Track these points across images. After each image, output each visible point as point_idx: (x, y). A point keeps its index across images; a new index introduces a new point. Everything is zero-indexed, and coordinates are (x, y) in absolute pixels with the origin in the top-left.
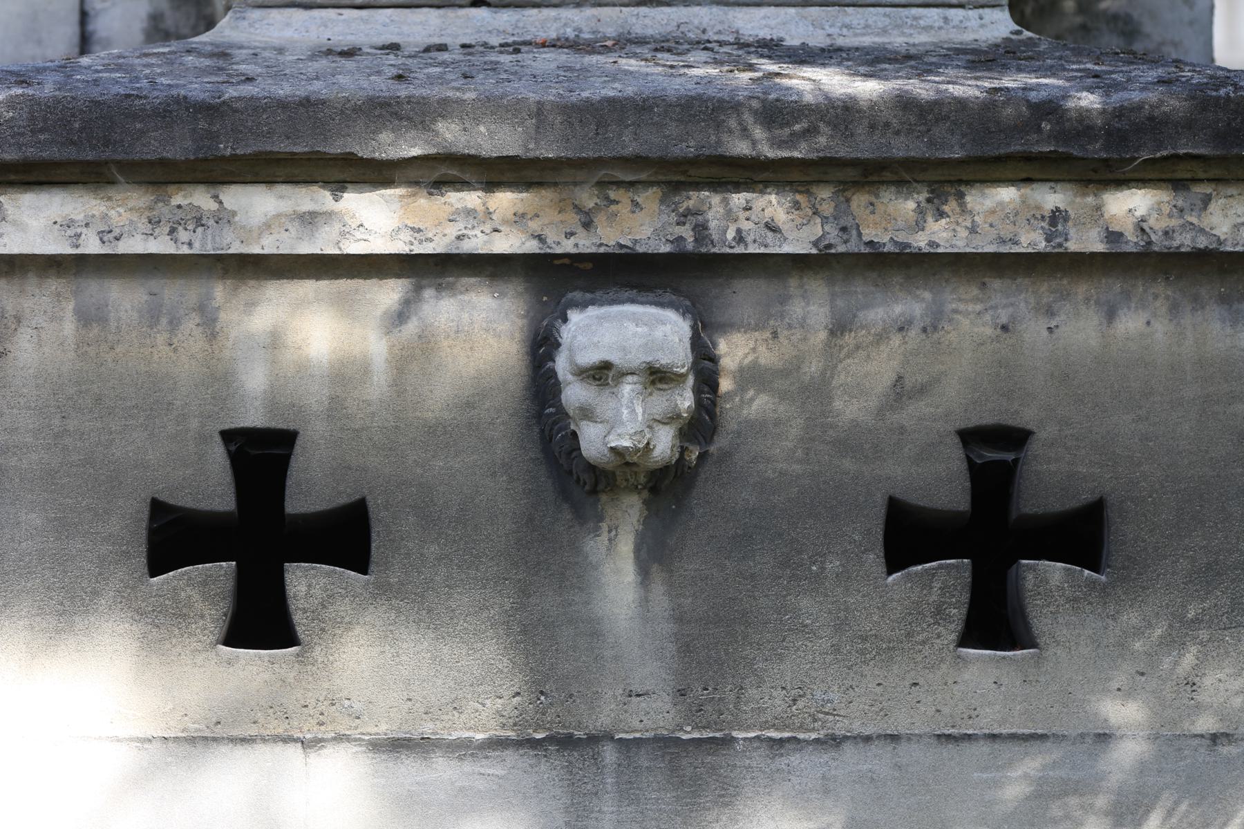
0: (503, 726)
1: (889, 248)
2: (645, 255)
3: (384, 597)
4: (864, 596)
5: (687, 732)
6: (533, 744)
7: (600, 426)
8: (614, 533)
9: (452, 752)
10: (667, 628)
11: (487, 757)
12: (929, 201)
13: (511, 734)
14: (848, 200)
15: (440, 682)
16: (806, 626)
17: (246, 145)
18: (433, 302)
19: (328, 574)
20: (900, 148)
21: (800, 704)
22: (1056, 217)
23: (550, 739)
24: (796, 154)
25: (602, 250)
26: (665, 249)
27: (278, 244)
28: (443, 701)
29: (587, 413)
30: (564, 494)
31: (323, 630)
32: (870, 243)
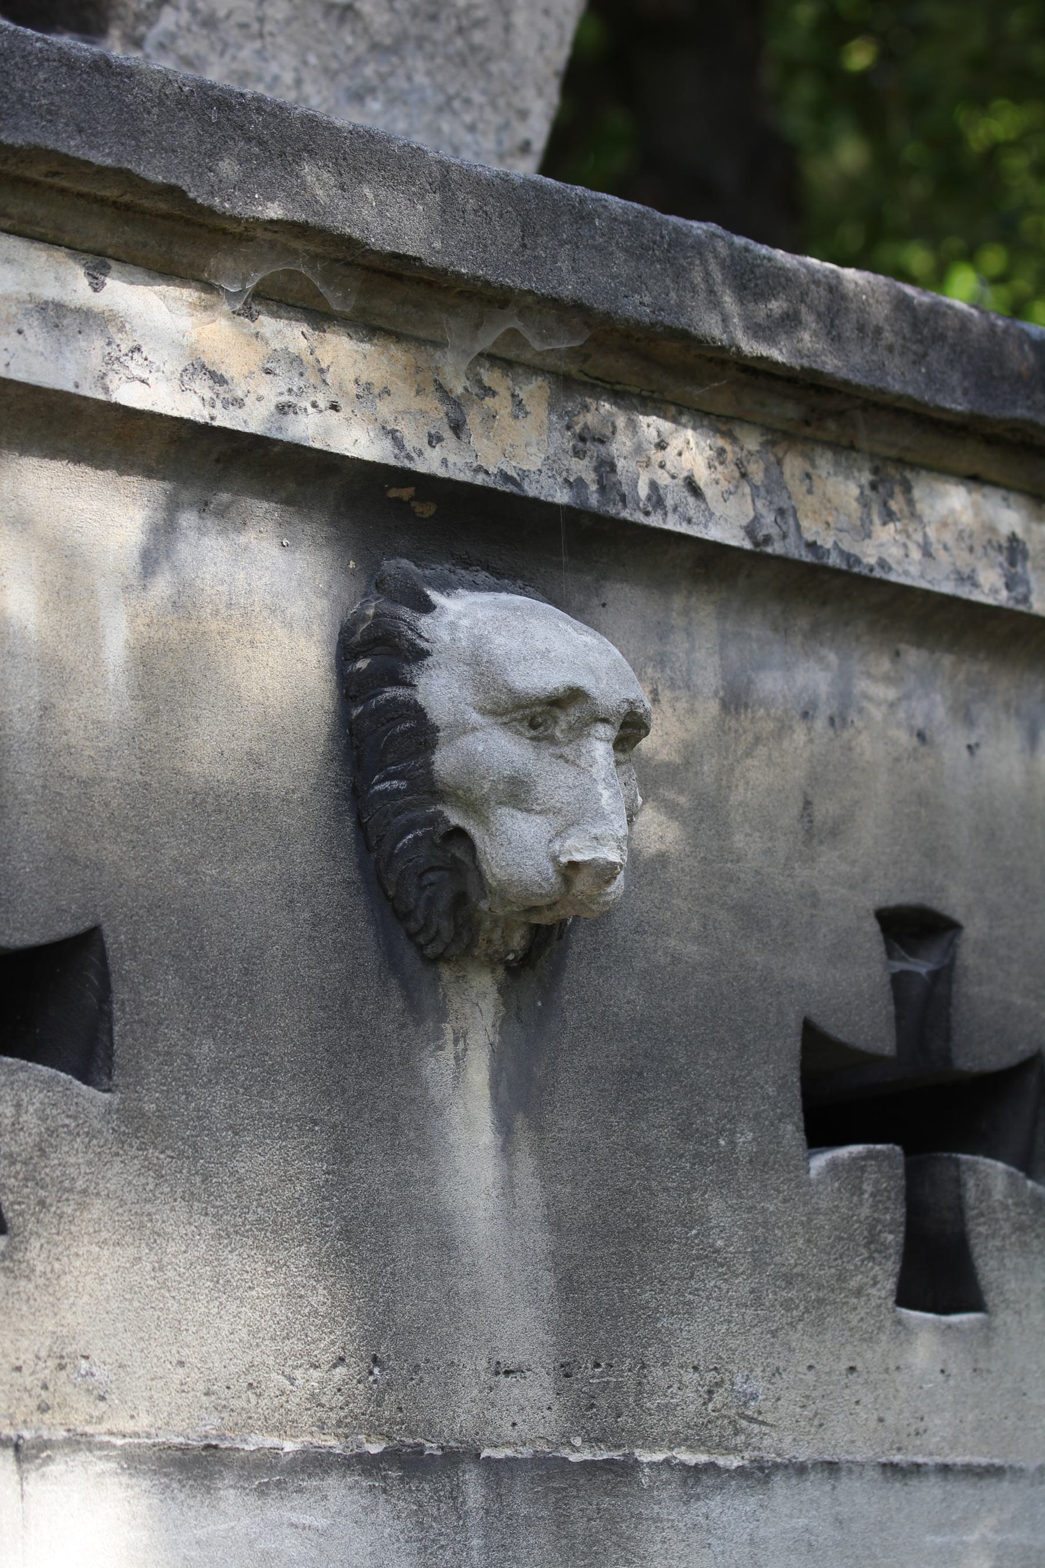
0: (322, 1426)
1: (834, 560)
2: (536, 501)
3: (136, 1143)
4: (785, 1201)
5: (575, 1449)
6: (366, 1464)
7: (539, 819)
8: (461, 1046)
9: (248, 1478)
10: (541, 1240)
11: (300, 1490)
12: (874, 486)
13: (332, 1442)
14: (779, 462)
15: (226, 1327)
16: (717, 1251)
17: (16, 128)
18: (192, 535)
19: (48, 1084)
20: (899, 379)
21: (718, 1399)
22: (1014, 550)
23: (392, 1456)
24: (778, 355)
25: (480, 480)
26: (562, 497)
27: (6, 357)
28: (232, 1368)
29: (517, 792)
30: (392, 962)
31: (42, 1203)
32: (812, 546)
